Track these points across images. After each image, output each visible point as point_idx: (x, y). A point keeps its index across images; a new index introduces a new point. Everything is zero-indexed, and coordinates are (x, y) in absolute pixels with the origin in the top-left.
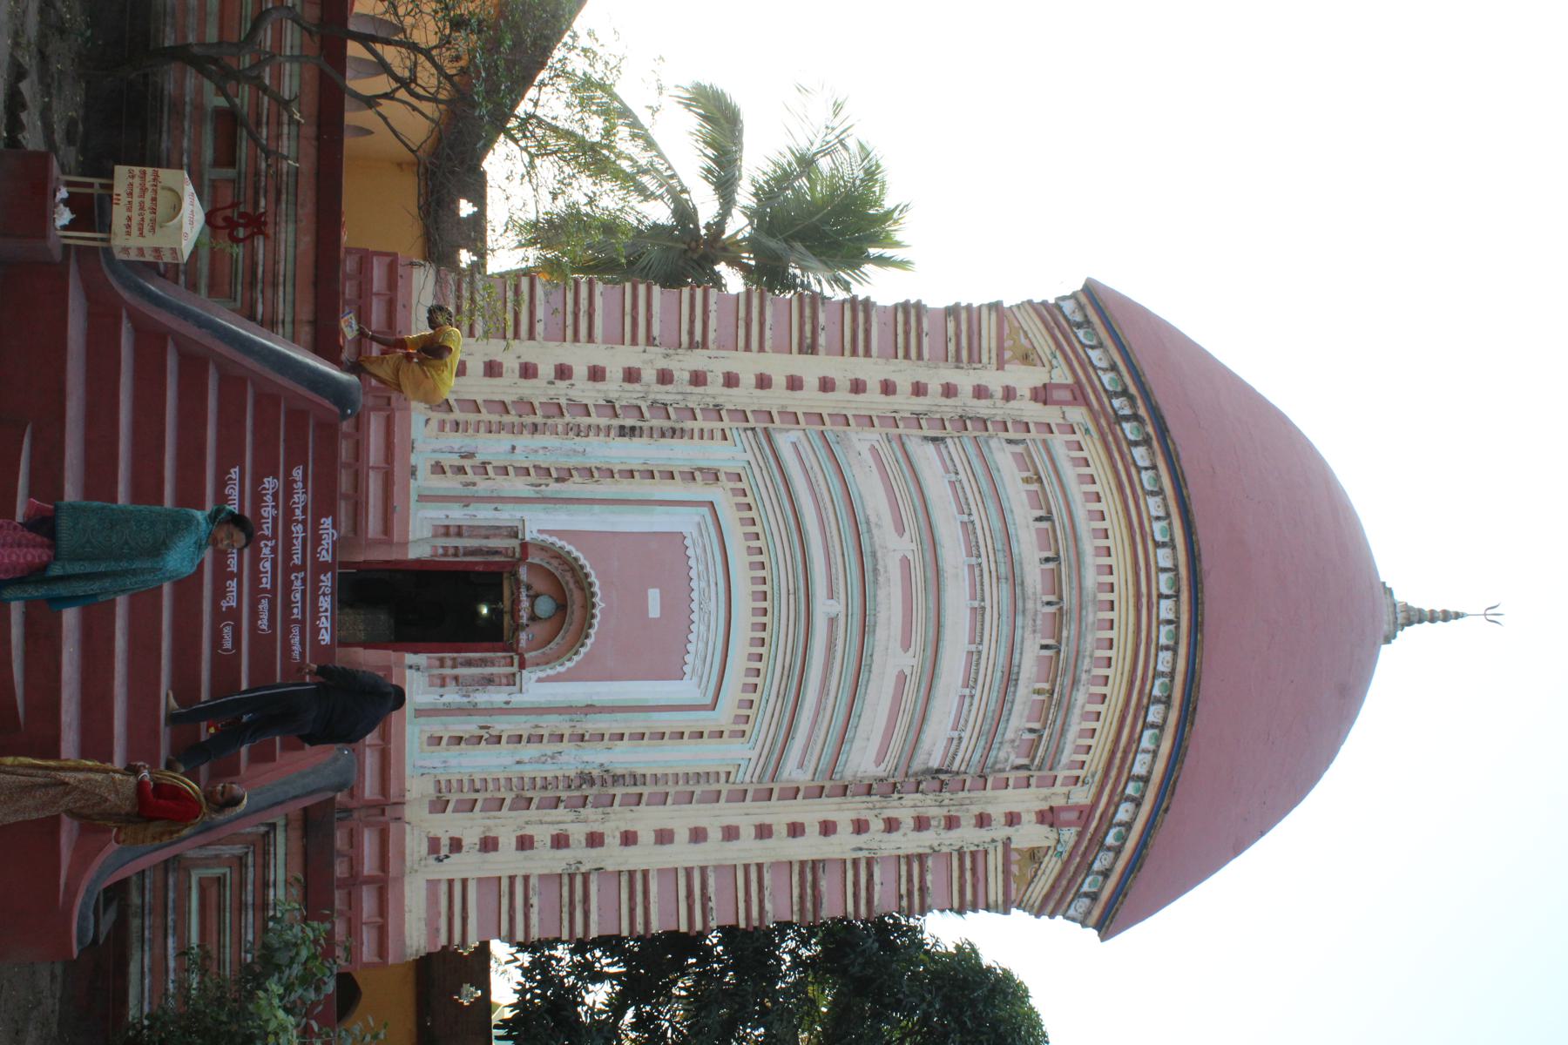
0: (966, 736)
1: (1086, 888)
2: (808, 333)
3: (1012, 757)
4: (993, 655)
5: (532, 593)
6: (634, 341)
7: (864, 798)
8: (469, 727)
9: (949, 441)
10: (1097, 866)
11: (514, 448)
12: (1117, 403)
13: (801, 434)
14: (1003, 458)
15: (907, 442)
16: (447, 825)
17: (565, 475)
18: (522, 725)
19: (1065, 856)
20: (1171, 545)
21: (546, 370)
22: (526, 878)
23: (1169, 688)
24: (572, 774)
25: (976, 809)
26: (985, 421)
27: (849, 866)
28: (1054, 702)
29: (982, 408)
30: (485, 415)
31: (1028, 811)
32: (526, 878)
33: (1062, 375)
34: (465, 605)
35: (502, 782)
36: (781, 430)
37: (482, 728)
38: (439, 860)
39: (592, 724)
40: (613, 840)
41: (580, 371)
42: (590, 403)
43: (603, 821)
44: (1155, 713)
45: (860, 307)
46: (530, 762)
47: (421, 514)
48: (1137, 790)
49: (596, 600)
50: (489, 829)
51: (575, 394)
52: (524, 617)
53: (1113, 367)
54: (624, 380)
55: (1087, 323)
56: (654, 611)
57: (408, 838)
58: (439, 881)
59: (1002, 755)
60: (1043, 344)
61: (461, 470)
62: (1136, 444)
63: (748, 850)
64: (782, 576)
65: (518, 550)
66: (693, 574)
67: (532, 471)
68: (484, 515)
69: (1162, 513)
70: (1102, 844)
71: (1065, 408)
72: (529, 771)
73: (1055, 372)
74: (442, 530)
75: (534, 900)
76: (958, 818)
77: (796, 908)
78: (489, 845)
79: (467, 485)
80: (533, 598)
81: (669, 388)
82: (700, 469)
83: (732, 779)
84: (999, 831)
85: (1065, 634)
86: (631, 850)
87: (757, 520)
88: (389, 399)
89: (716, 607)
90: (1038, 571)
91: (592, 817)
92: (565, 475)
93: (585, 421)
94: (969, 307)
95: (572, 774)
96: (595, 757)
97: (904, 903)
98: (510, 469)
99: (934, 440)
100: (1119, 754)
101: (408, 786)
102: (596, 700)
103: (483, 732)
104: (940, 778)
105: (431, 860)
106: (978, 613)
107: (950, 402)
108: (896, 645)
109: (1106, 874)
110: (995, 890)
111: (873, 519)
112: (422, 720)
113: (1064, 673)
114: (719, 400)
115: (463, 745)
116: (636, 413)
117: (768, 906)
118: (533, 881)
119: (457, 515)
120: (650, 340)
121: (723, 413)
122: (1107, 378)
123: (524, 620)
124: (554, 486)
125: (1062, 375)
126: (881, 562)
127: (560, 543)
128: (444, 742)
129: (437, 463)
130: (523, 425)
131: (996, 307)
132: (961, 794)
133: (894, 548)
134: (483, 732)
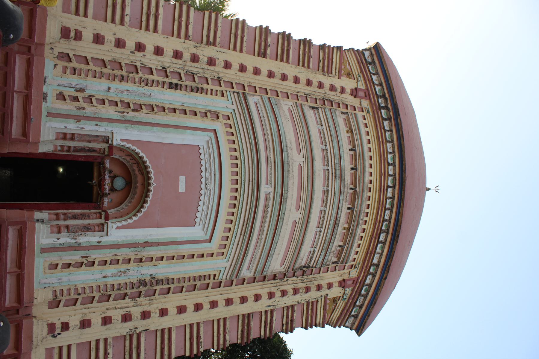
0: (317, 250)
1: (353, 313)
2: (263, 47)
3: (333, 258)
4: (331, 212)
5: (112, 175)
6: (179, 36)
7: (273, 281)
8: (75, 257)
9: (320, 109)
10: (358, 303)
11: (109, 88)
12: (380, 100)
13: (259, 98)
14: (340, 120)
15: (303, 107)
16: (58, 316)
17: (139, 108)
18: (107, 254)
19: (347, 300)
20: (394, 165)
21: (131, 44)
22: (106, 340)
23: (388, 226)
24: (135, 281)
25: (316, 283)
26: (332, 102)
27: (263, 314)
28: (349, 233)
29: (332, 95)
30: (92, 67)
31: (335, 282)
32: (106, 340)
33: (361, 85)
34: (81, 182)
35: (95, 288)
36: (251, 95)
37: (83, 257)
38: (54, 336)
39: (147, 252)
40: (155, 315)
41: (150, 48)
42: (153, 67)
43: (150, 304)
44: (383, 236)
45: (286, 38)
46: (111, 275)
47: (48, 125)
48: (374, 270)
49: (152, 181)
50: (85, 315)
51: (145, 61)
52: (107, 188)
53: (381, 84)
54: (173, 57)
55: (373, 62)
56: (182, 189)
57: (35, 328)
58: (54, 348)
59: (330, 258)
60: (356, 70)
61: (76, 99)
62: (385, 119)
63: (222, 312)
64: (247, 172)
65: (107, 150)
66: (203, 168)
67: (119, 104)
68: (89, 128)
69: (391, 151)
70: (360, 293)
71: (362, 100)
72: (110, 281)
73: (359, 83)
74: (61, 136)
75: (110, 351)
76: (310, 287)
77: (239, 337)
78: (85, 324)
79: (79, 108)
80: (113, 178)
81: (196, 64)
82: (210, 111)
83: (216, 278)
84: (324, 292)
85: (356, 203)
86: (165, 318)
87: (236, 142)
88: (29, 48)
89: (213, 187)
90: (349, 174)
91: (144, 303)
92: (139, 108)
93: (150, 77)
94: (329, 46)
95: (135, 281)
96: (147, 271)
97: (284, 328)
98: (106, 101)
99: (314, 108)
100: (370, 253)
101: (35, 296)
102: (150, 239)
103: (84, 260)
104: (304, 270)
105: (50, 338)
106: (326, 192)
107: (320, 91)
108: (294, 208)
109: (361, 307)
110: (319, 318)
111: (289, 145)
112: (46, 254)
113: (354, 221)
114: (221, 75)
115: (71, 268)
116: (178, 76)
117: (228, 337)
118: (109, 340)
119: (72, 127)
120: (187, 37)
121: (222, 82)
122: (378, 88)
123: (107, 191)
124: (132, 114)
125: (361, 85)
126: (291, 167)
127: (133, 148)
128: (59, 267)
129: (61, 93)
130: (115, 76)
131: (340, 48)
132: (311, 276)
133: (296, 159)
134: (84, 260)
